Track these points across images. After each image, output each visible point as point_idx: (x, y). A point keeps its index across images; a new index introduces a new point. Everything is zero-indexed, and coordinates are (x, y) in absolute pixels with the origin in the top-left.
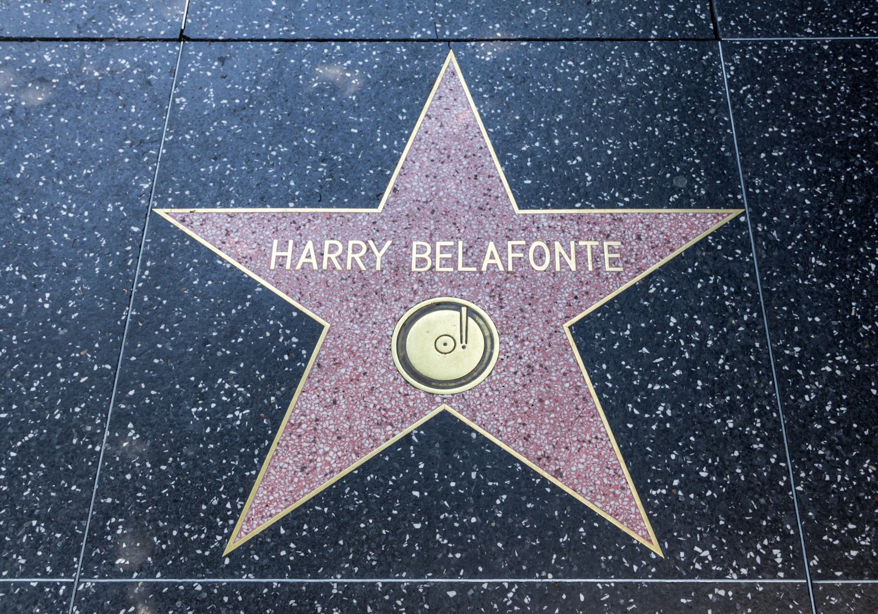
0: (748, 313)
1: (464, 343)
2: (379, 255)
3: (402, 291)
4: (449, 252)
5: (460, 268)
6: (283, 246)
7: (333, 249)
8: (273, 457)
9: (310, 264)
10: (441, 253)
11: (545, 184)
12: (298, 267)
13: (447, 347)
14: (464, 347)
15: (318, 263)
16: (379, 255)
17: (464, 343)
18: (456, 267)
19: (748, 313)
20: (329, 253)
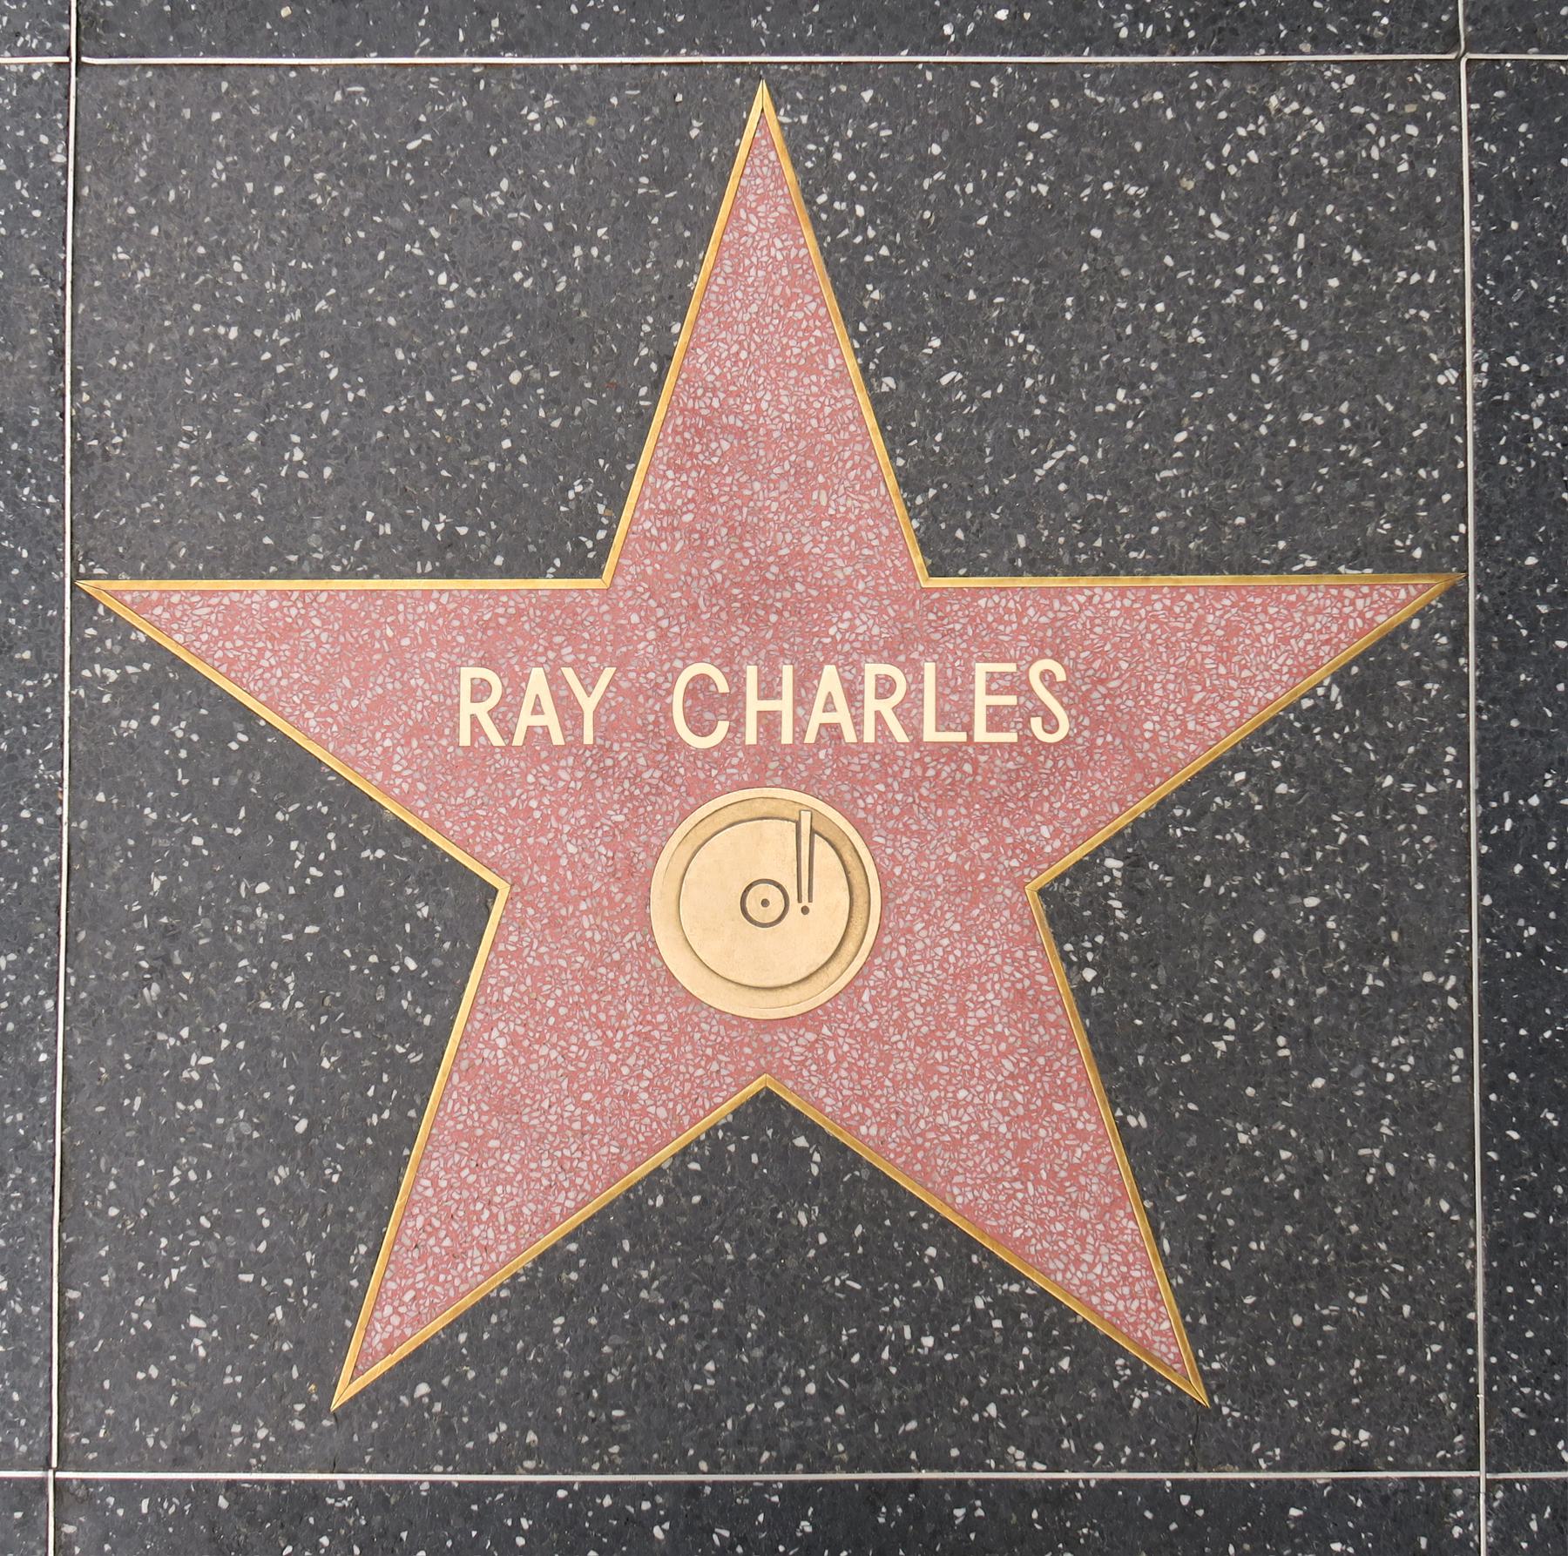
0: (1014, 835)
1: (805, 902)
2: (588, 704)
3: (646, 781)
4: (1009, 691)
5: (981, 734)
6: (769, 690)
7: (885, 688)
9: (837, 726)
10: (989, 692)
11: (977, 511)
12: (810, 738)
13: (757, 928)
14: (805, 910)
15: (797, 721)
16: (588, 704)
17: (805, 902)
18: (968, 728)
19: (1014, 835)
20: (879, 696)
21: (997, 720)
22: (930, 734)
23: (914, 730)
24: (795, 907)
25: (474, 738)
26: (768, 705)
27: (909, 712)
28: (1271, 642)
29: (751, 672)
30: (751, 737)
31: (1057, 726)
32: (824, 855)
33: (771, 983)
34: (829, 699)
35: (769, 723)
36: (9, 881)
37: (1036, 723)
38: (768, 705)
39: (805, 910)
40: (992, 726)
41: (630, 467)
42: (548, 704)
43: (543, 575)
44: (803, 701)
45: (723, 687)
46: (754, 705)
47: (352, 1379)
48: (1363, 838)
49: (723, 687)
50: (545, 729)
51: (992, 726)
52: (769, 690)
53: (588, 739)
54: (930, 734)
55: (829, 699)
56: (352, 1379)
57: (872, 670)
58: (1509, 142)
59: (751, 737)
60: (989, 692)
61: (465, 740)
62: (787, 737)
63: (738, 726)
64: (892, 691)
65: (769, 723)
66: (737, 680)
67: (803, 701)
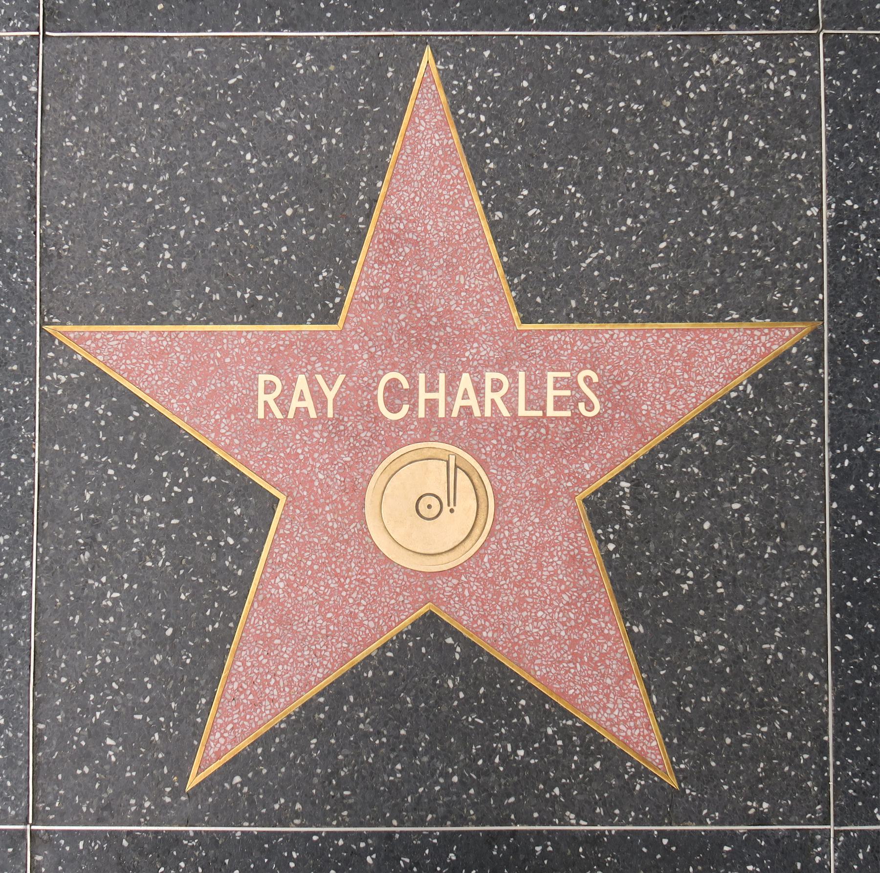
0: (569, 469)
1: (452, 506)
2: (330, 395)
3: (362, 438)
4: (566, 387)
5: (551, 412)
6: (432, 387)
7: (497, 386)
8: (649, 724)
9: (470, 408)
10: (555, 388)
11: (548, 287)
12: (455, 414)
13: (425, 520)
14: (452, 511)
15: (447, 404)
16: (330, 395)
17: (452, 506)
18: (544, 408)
19: (569, 469)
20: (493, 391)
21: (559, 404)
22: (522, 412)
23: (513, 410)
24: (446, 509)
25: (266, 414)
26: (431, 396)
27: (510, 400)
28: (713, 360)
29: (422, 377)
30: (421, 414)
31: (593, 407)
32: (463, 480)
33: (433, 552)
34: (466, 392)
35: (432, 405)
36: (5, 494)
37: (581, 406)
38: (431, 396)
39: (452, 511)
40: (557, 408)
41: (353, 262)
42: (307, 395)
43: (305, 323)
44: (450, 393)
45: (406, 385)
46: (423, 396)
47: (198, 774)
48: (765, 470)
49: (406, 385)
50: (306, 409)
51: (557, 408)
52: (432, 387)
53: (330, 414)
54: (522, 412)
55: (466, 392)
56: (198, 774)
57: (489, 376)
58: (847, 80)
59: (421, 414)
60: (555, 388)
61: (261, 415)
62: (442, 414)
63: (414, 407)
64: (500, 387)
65: (432, 405)
66: (413, 381)
67: (450, 393)
